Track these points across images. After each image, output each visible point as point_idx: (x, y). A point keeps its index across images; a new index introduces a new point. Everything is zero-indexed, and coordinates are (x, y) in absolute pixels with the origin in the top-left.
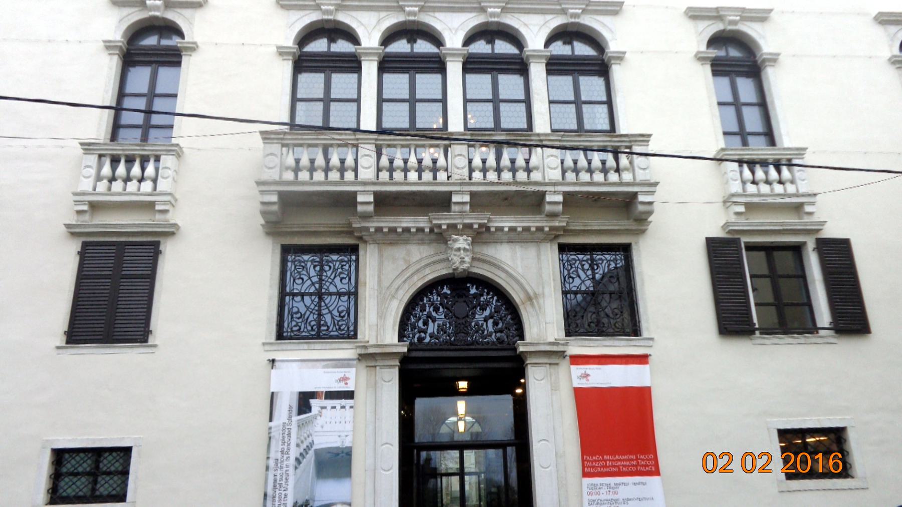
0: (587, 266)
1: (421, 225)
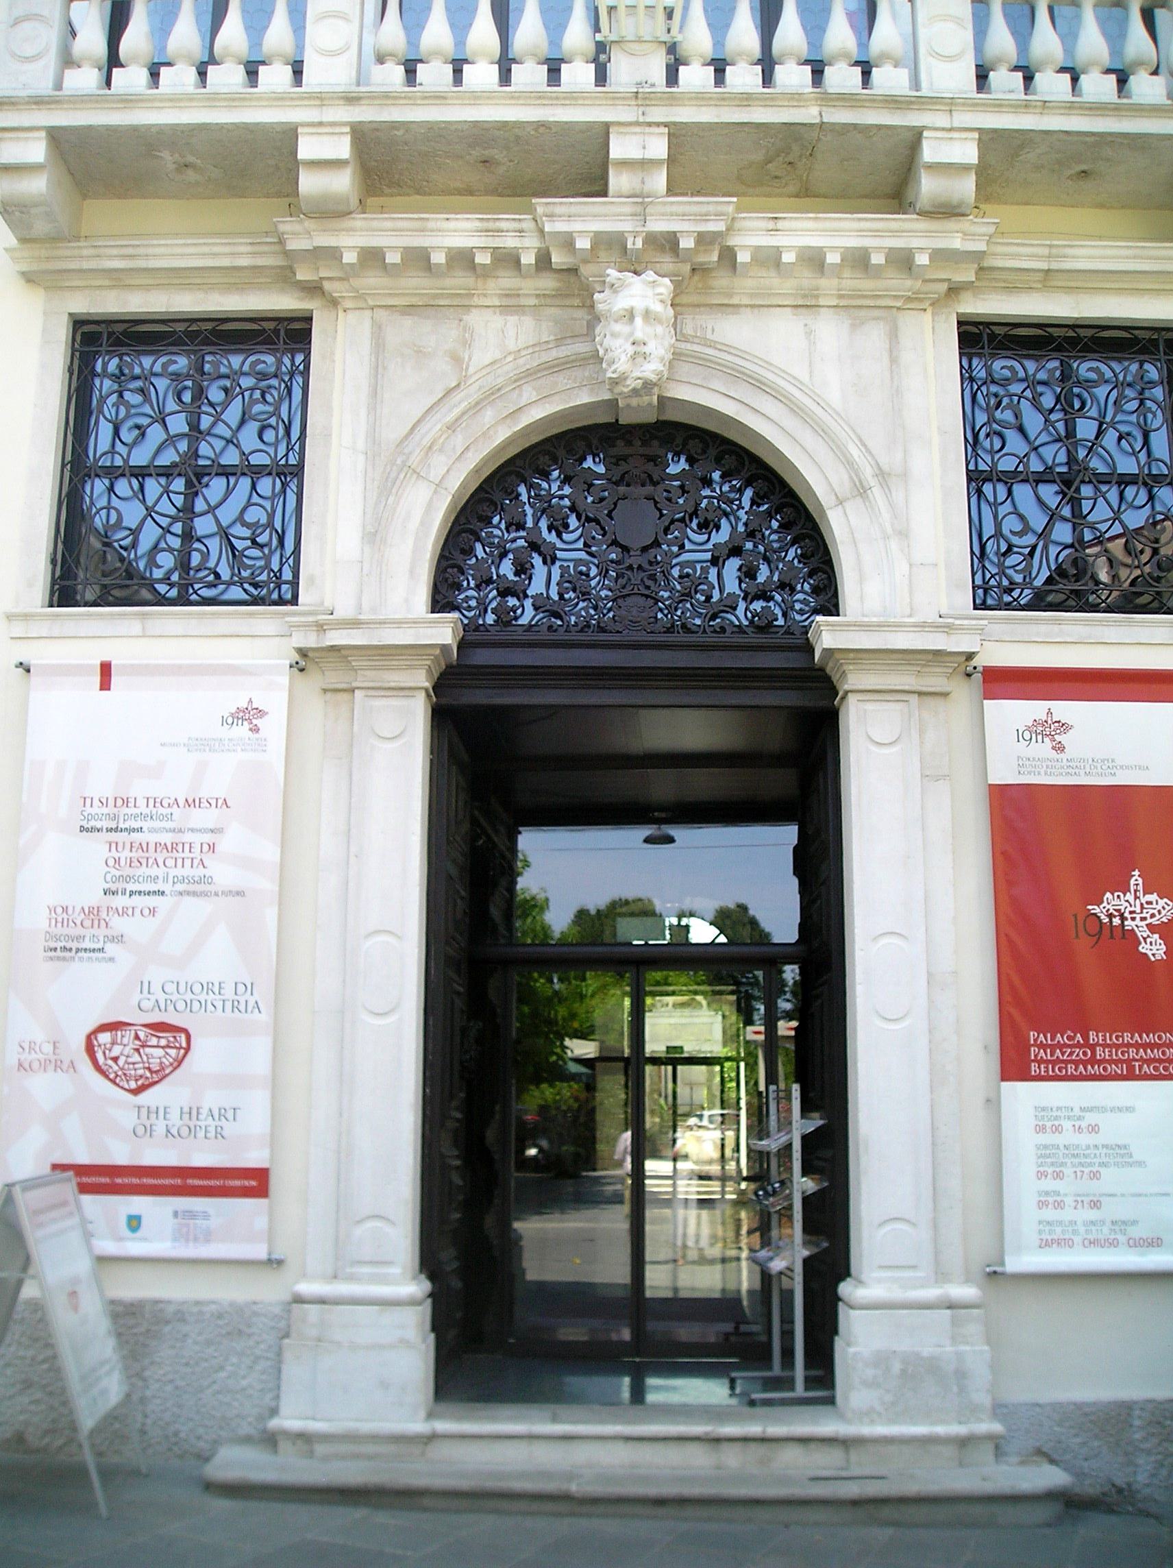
0: (1048, 401)
1: (510, 242)
